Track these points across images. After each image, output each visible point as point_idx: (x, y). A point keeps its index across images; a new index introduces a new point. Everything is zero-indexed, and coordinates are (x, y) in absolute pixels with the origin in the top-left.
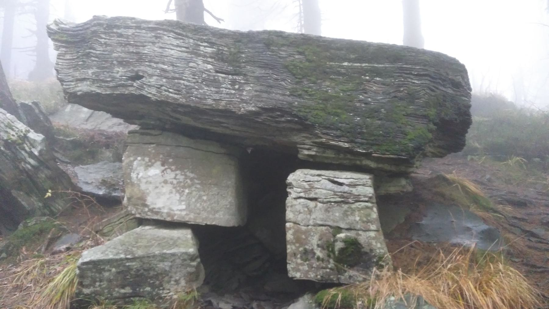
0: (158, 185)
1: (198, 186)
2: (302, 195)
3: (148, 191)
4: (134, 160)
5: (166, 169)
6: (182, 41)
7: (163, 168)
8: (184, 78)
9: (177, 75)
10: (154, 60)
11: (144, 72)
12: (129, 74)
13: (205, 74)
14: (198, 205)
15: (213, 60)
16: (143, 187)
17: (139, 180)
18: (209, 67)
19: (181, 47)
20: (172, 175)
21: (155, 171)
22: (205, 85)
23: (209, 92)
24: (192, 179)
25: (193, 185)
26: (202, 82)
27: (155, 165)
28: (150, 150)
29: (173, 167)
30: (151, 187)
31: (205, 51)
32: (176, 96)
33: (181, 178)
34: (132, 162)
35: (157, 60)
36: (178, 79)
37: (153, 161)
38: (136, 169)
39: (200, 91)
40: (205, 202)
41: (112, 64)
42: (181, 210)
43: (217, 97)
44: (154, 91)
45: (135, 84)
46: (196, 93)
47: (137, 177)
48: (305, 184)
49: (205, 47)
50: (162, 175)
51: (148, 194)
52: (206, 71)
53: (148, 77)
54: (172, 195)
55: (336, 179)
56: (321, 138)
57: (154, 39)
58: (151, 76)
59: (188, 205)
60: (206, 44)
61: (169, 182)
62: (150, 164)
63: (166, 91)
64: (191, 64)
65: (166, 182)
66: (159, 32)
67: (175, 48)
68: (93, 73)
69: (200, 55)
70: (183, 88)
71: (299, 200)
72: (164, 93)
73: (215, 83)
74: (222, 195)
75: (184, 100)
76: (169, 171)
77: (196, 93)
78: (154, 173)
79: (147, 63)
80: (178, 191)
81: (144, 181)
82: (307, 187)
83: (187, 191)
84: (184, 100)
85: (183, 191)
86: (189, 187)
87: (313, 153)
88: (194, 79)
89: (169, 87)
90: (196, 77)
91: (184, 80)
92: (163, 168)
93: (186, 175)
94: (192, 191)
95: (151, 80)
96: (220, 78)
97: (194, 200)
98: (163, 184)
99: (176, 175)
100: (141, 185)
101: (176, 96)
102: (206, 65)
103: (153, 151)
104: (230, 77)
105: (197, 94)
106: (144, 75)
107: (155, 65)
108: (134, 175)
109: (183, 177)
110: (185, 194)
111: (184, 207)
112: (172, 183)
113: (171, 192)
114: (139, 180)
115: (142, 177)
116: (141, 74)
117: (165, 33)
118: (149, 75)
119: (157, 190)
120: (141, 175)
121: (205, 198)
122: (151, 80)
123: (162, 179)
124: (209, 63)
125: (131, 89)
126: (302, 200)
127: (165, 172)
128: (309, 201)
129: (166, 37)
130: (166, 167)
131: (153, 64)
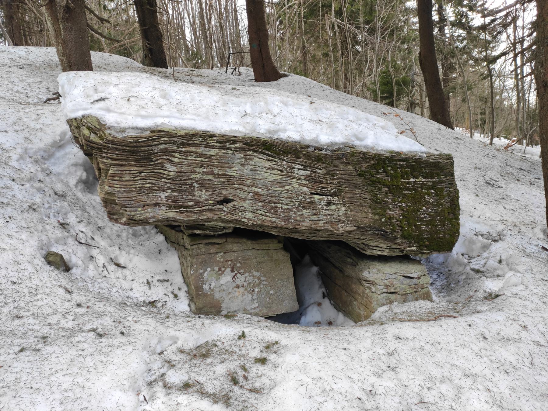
0: (230, 291)
1: (265, 283)
2: (385, 290)
3: (222, 298)
4: (204, 272)
5: (236, 274)
6: (274, 163)
7: (233, 274)
8: (281, 201)
9: (273, 199)
10: (245, 182)
11: (234, 195)
12: (217, 199)
13: (302, 196)
14: (268, 299)
15: (307, 182)
16: (217, 296)
17: (213, 290)
18: (305, 189)
19: (273, 169)
20: (242, 278)
21: (226, 278)
22: (302, 207)
23: (308, 214)
24: (259, 278)
25: (260, 283)
26: (299, 205)
27: (225, 273)
28: (218, 259)
29: (242, 271)
30: (224, 294)
31: (299, 174)
32: (274, 220)
33: (250, 279)
34: (202, 274)
35: (248, 182)
36: (274, 202)
37: (223, 269)
38: (207, 280)
39: (299, 213)
40: (273, 295)
41: (191, 186)
42: (255, 309)
43: (315, 218)
44: (250, 215)
45: (225, 209)
46: (294, 215)
47: (210, 288)
48: (385, 281)
49: (299, 169)
50: (234, 281)
51: (223, 301)
52: (302, 193)
53: (240, 201)
54: (245, 297)
55: (409, 275)
56: (401, 245)
57: (243, 160)
58: (243, 200)
59: (260, 302)
60: (300, 167)
61: (241, 286)
62: (220, 272)
63: (262, 215)
64: (287, 187)
65: (238, 287)
66: (248, 153)
67: (268, 171)
68: (168, 198)
69: (294, 178)
70: (281, 212)
71: (382, 295)
72: (261, 217)
73: (312, 205)
74: (285, 286)
75: (283, 223)
76: (239, 275)
77: (294, 215)
78: (226, 281)
79: (236, 186)
80: (249, 292)
81: (217, 290)
82: (388, 284)
83: (256, 290)
84: (283, 223)
85: (253, 291)
86: (258, 285)
87: (386, 254)
88: (291, 202)
89: (266, 211)
90: (294, 200)
91: (281, 204)
92: (233, 274)
93: (254, 276)
94: (261, 289)
95: (245, 204)
96: (316, 200)
97: (263, 296)
98: (235, 289)
99: (246, 278)
100: (215, 294)
101: (274, 220)
102: (301, 188)
103: (222, 260)
104: (326, 198)
105: (296, 217)
106: (235, 199)
107: (246, 189)
108: (206, 287)
109: (252, 278)
110: (256, 293)
111: (257, 305)
112: (243, 286)
113: (243, 295)
114: (213, 290)
115: (214, 287)
116: (231, 198)
117: (255, 154)
118: (241, 199)
119: (230, 296)
120: (213, 285)
121: (272, 292)
122: (245, 204)
123: (234, 285)
124: (304, 185)
125: (220, 214)
126: (385, 295)
127: (236, 277)
128: (390, 295)
129: (256, 158)
130: (236, 272)
131: (244, 187)
